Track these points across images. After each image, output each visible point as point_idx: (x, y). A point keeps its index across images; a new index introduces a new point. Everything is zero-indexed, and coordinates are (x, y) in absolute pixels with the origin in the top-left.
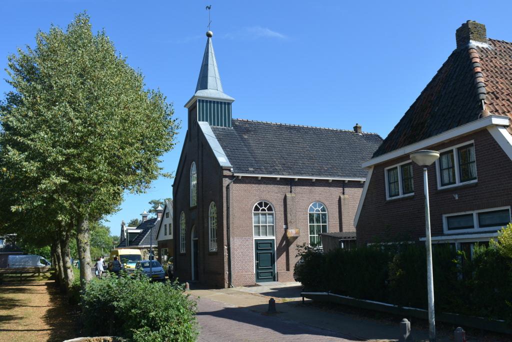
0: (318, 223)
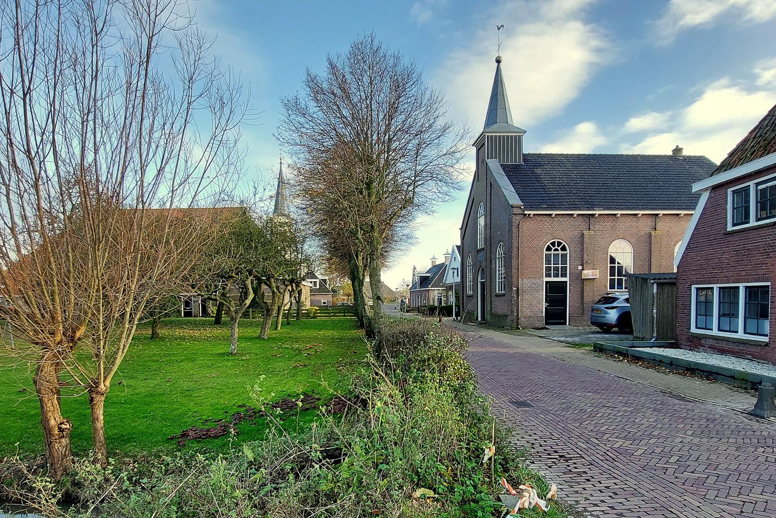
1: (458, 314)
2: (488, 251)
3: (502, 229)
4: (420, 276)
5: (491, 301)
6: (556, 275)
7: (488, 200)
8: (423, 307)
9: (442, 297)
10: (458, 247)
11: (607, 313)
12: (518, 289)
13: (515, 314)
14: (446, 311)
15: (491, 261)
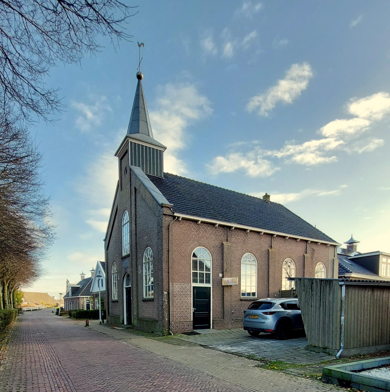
0: (195, 270)
1: (104, 317)
2: (134, 257)
3: (149, 233)
4: (71, 287)
5: (138, 306)
6: (202, 281)
7: (133, 206)
8: (73, 311)
9: (90, 303)
10: (102, 263)
11: (266, 318)
12: (169, 293)
13: (167, 319)
14: (93, 315)
15: (137, 267)
